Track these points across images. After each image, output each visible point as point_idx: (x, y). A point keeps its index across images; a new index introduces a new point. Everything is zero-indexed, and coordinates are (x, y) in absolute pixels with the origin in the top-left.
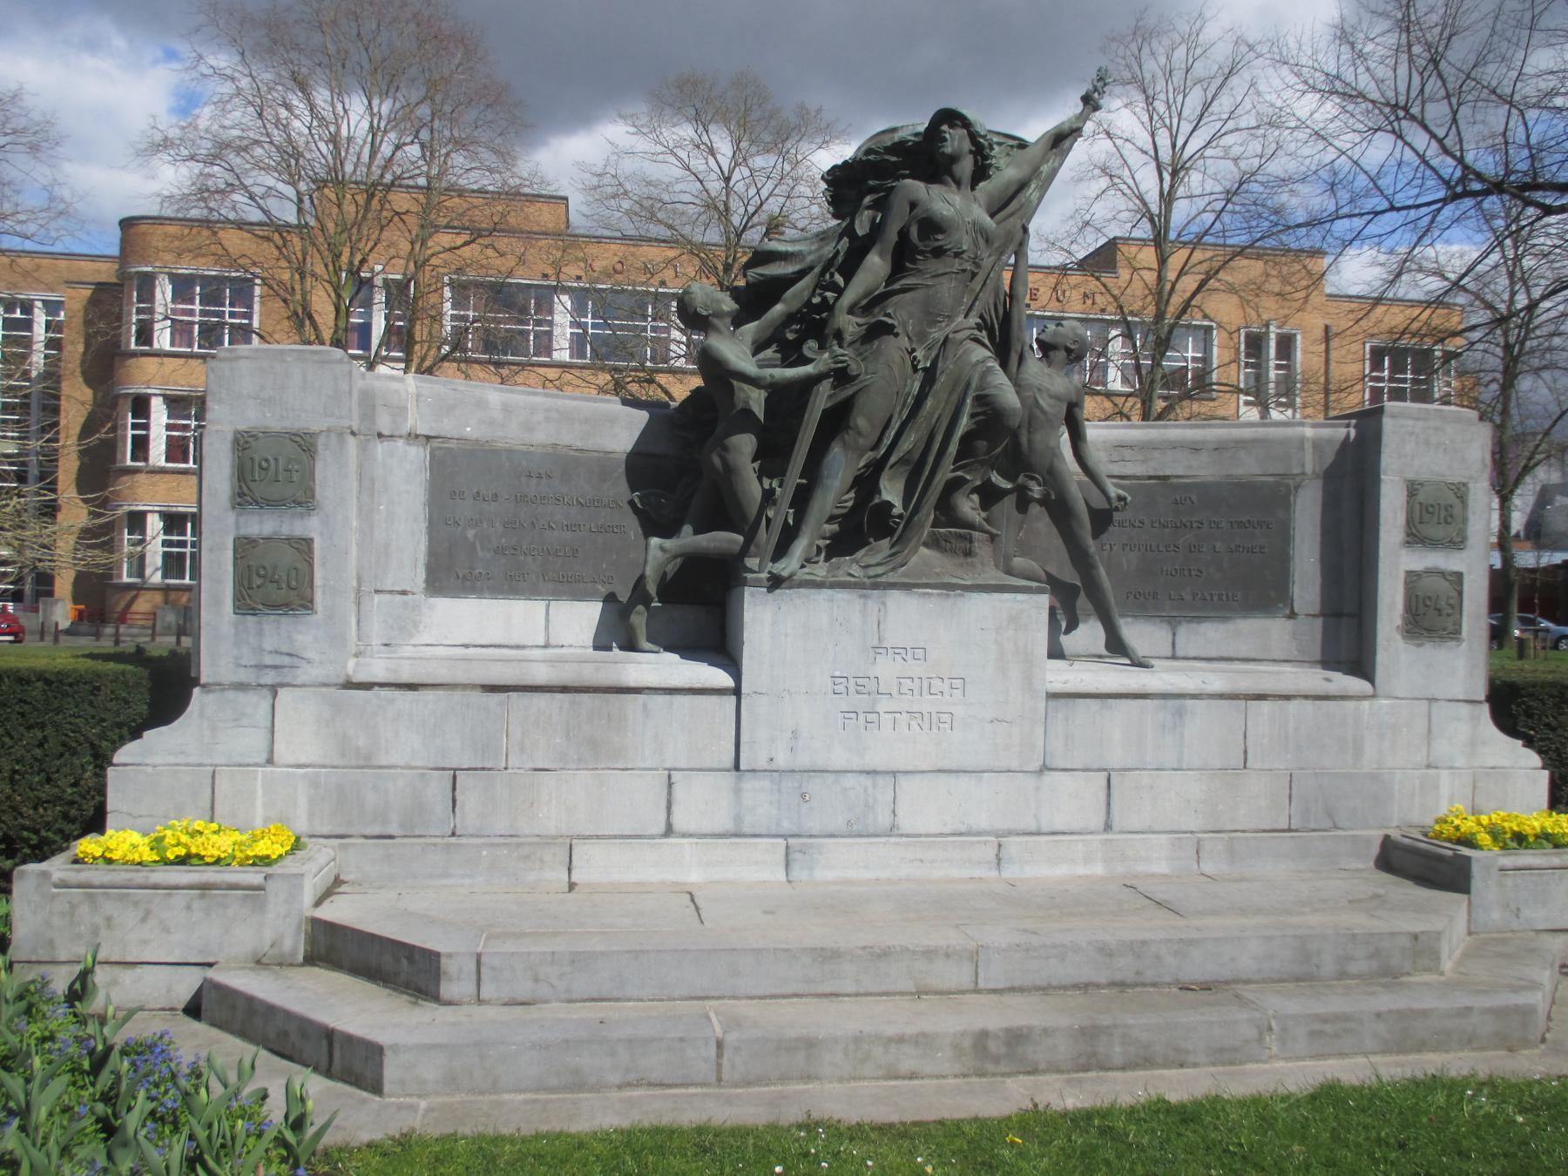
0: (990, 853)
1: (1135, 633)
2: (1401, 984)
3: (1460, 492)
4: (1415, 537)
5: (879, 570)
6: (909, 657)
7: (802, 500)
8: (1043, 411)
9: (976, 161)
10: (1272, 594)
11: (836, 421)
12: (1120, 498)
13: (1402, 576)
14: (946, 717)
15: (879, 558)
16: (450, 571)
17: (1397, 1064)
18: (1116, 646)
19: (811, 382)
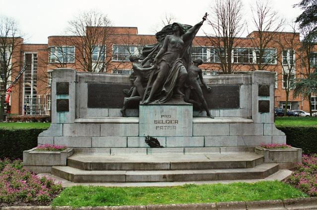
0: (183, 150)
1: (212, 112)
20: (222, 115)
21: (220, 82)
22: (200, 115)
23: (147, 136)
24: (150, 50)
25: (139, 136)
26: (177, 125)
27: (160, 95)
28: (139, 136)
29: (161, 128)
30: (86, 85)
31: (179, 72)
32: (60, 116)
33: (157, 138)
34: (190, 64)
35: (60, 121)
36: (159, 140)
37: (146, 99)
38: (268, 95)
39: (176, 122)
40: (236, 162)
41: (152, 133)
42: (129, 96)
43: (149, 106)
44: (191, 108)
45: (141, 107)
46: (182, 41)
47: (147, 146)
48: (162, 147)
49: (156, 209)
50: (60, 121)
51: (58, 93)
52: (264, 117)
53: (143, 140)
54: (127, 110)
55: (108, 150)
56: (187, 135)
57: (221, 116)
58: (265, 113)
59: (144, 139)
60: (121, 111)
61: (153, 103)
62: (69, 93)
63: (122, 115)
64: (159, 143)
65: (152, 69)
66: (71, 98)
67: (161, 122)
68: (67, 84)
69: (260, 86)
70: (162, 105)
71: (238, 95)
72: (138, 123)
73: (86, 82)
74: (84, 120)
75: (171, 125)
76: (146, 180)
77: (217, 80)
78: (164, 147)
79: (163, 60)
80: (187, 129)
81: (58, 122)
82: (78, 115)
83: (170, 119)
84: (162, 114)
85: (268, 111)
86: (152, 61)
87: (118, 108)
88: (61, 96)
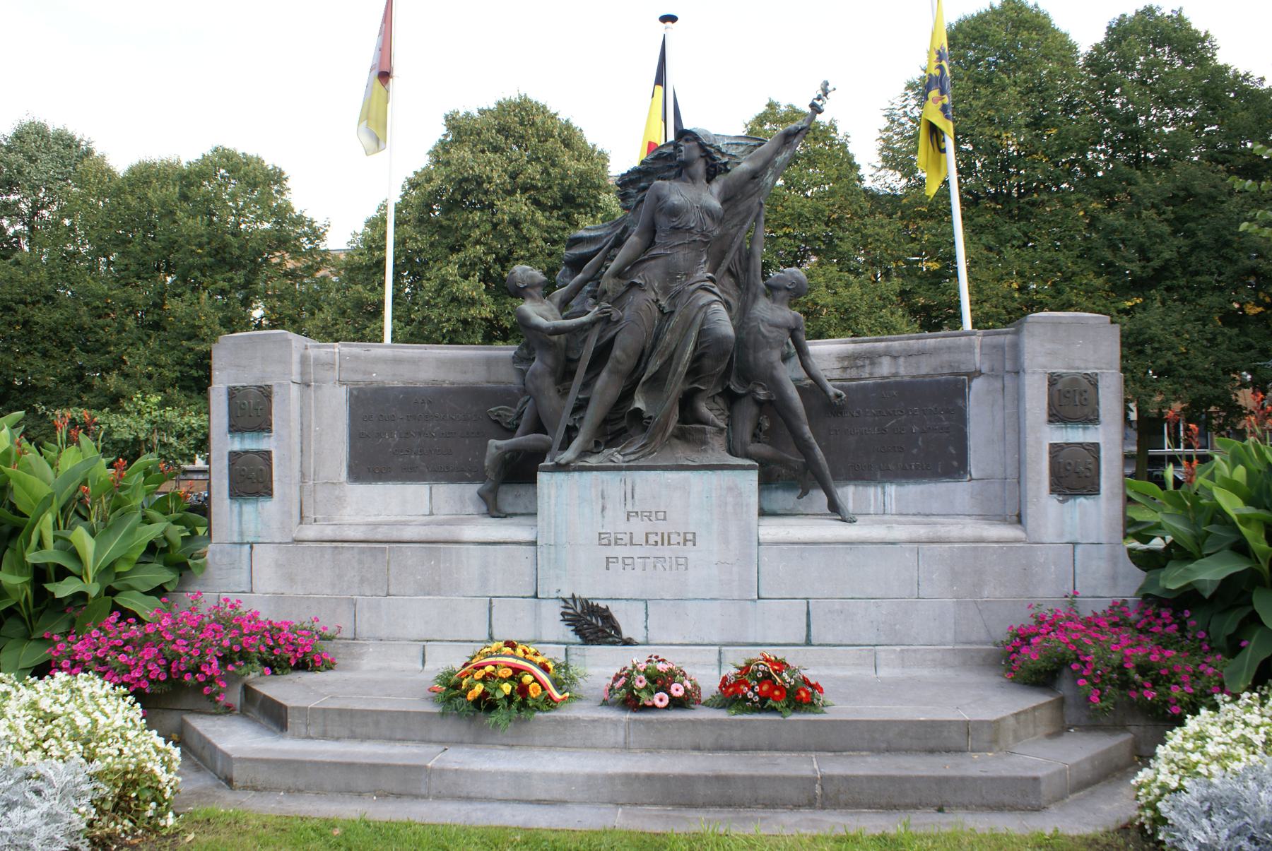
0: (715, 658)
1: (849, 494)
2: (563, 722)
3: (1093, 381)
4: (235, 428)
5: (632, 457)
6: (653, 518)
7: (581, 406)
8: (764, 336)
9: (707, 163)
10: (955, 463)
11: (602, 354)
12: (838, 396)
13: (1047, 448)
14: (681, 561)
15: (633, 449)
16: (370, 462)
17: (947, 824)
18: (835, 508)
19: (582, 328)
20: (892, 507)
21: (885, 368)
22: (801, 509)
23: (567, 595)
24: (593, 248)
25: (536, 596)
26: (690, 552)
27: (624, 430)
28: (536, 596)
29: (626, 563)
30: (342, 393)
31: (702, 333)
32: (241, 514)
33: (609, 603)
34: (755, 297)
35: (241, 534)
36: (620, 613)
37: (565, 446)
38: (1091, 419)
39: (689, 539)
40: (848, 721)
41: (592, 588)
42: (510, 432)
43: (576, 474)
44: (749, 481)
45: (542, 477)
46: (715, 203)
47: (571, 636)
48: (629, 642)
49: (839, 840)
50: (241, 534)
51: (235, 428)
52: (1077, 515)
53: (553, 611)
54: (503, 488)
55: (415, 650)
56: (736, 595)
57: (885, 514)
58: (1081, 500)
59: (555, 609)
60: (481, 495)
61: (593, 461)
62: (274, 427)
63: (484, 509)
64: (618, 631)
65: (592, 324)
66: (278, 444)
67: (626, 538)
68: (265, 393)
69: (1053, 380)
70: (629, 468)
71: (961, 419)
72: (534, 543)
73: (341, 383)
74: (329, 532)
75: (665, 551)
76: (513, 794)
77: (873, 357)
78: (637, 644)
79: (635, 284)
80: (735, 569)
81: (236, 539)
82: (309, 513)
83: (662, 527)
84: (629, 508)
85: (1090, 488)
86: (597, 297)
87: (471, 481)
88: (242, 439)
